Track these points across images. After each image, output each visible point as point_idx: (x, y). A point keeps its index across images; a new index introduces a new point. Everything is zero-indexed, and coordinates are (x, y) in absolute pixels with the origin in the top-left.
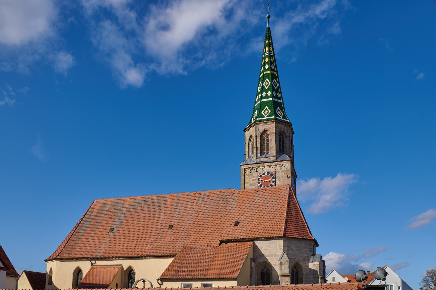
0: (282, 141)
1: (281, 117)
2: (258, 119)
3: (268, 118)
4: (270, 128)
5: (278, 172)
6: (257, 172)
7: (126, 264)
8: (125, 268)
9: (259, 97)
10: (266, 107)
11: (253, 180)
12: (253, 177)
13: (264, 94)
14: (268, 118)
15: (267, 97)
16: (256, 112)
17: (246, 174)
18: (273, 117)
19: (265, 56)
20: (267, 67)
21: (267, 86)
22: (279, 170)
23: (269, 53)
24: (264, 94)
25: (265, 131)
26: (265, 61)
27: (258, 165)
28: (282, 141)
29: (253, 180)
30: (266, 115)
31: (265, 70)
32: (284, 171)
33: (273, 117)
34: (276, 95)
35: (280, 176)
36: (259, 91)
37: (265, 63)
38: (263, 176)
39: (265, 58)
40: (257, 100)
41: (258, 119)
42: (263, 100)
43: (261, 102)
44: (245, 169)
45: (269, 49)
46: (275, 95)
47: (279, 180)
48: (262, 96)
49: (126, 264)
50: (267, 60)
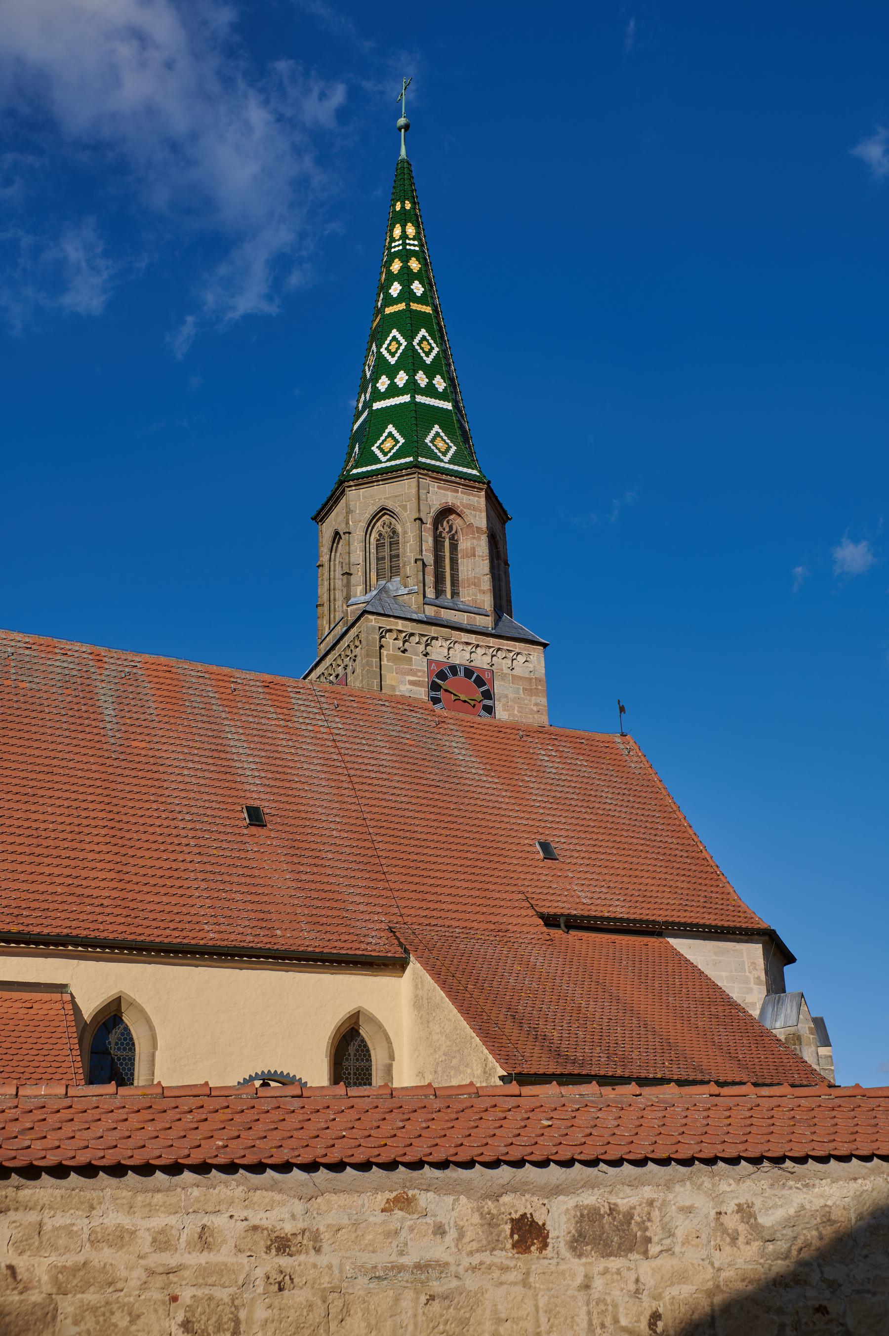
3: (393, 463)
4: (469, 506)
5: (504, 677)
6: (426, 655)
7: (92, 984)
8: (89, 1008)
10: (391, 428)
11: (412, 683)
12: (412, 672)
13: (383, 384)
15: (393, 391)
17: (384, 652)
18: (411, 459)
20: (395, 289)
21: (427, 354)
22: (506, 671)
23: (404, 244)
24: (383, 384)
25: (446, 512)
26: (389, 272)
27: (433, 631)
29: (412, 683)
30: (385, 454)
31: (390, 301)
32: (521, 678)
34: (430, 385)
35: (511, 696)
37: (392, 278)
38: (450, 675)
39: (390, 262)
40: (360, 405)
41: (355, 471)
43: (413, 402)
44: (384, 633)
45: (404, 231)
47: (506, 708)
48: (375, 390)
49: (92, 984)
50: (396, 266)
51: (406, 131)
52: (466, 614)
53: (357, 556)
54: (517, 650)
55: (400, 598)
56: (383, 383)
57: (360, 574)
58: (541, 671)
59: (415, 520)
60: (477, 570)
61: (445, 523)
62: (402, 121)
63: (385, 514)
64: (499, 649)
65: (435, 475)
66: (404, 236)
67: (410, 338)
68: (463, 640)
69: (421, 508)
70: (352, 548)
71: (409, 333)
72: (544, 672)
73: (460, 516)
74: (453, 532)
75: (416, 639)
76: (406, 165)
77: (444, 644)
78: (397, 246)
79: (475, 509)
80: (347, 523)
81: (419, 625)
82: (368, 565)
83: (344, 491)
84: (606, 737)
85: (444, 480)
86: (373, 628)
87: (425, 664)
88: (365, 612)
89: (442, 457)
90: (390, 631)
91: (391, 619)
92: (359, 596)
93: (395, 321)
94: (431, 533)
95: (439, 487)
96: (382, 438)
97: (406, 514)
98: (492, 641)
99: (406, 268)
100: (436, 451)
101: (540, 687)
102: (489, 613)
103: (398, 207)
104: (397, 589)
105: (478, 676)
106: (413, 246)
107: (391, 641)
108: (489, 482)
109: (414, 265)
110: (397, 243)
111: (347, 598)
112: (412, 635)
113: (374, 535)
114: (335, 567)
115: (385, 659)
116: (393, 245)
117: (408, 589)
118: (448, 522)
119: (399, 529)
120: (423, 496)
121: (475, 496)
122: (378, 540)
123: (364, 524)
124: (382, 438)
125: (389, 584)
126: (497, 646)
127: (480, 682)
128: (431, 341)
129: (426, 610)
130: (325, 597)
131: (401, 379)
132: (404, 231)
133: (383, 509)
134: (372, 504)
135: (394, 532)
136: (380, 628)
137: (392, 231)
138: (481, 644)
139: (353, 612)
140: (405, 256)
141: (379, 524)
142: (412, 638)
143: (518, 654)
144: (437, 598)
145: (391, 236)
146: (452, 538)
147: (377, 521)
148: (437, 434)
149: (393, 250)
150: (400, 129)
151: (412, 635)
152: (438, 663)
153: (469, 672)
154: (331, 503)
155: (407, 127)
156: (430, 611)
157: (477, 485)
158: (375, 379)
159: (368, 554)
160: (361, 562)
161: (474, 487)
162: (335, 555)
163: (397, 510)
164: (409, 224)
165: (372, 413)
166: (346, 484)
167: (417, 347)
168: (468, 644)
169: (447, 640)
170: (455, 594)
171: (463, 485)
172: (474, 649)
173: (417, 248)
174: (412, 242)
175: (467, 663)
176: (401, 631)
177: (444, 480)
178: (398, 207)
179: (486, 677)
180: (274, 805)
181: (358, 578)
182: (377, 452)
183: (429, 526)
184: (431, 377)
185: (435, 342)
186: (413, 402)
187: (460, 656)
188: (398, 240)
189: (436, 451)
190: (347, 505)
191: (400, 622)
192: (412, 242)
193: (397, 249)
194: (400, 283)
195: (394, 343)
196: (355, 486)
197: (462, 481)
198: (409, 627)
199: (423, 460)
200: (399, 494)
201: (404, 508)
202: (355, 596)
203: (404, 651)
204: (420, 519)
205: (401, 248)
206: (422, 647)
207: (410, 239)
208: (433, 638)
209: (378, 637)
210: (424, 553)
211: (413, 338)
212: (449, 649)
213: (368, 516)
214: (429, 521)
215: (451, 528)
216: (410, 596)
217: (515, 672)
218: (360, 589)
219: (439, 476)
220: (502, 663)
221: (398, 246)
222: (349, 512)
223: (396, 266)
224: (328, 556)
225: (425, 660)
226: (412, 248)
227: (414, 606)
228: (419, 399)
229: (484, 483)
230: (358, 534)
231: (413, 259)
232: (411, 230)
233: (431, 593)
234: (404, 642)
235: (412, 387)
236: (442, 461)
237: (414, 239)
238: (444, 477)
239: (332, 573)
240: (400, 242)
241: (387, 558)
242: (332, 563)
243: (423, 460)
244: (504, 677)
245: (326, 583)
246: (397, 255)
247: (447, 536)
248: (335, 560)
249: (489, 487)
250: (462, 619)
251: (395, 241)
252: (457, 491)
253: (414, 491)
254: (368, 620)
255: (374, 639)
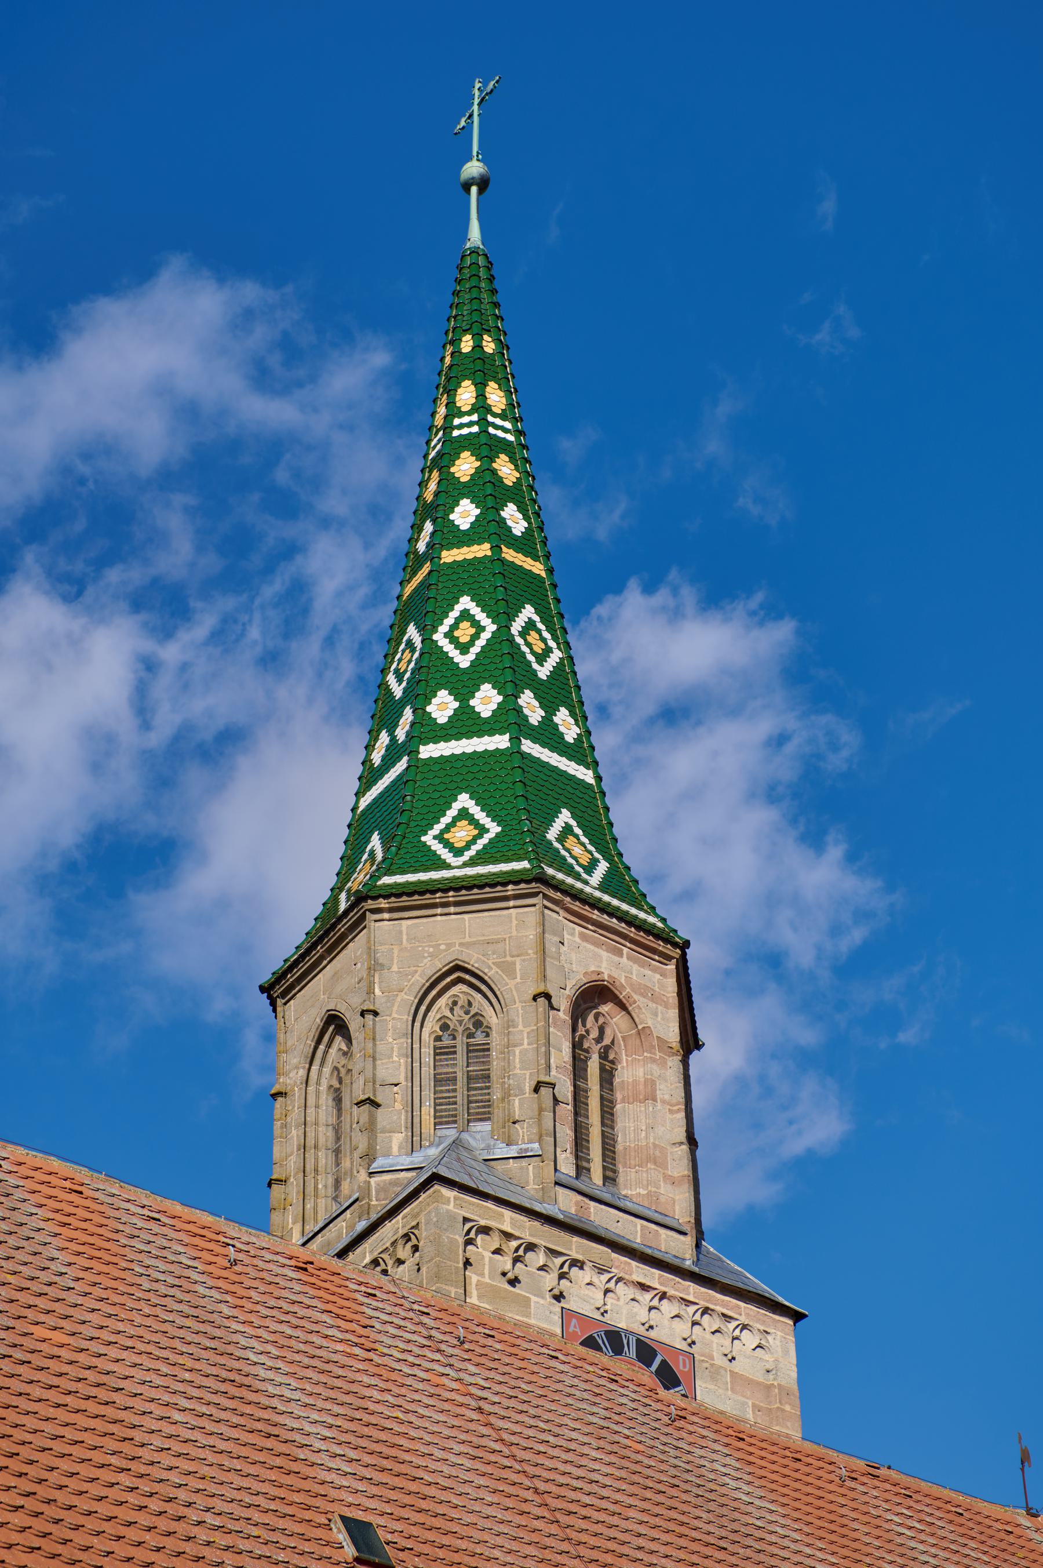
0: (593, 1065)
1: (596, 878)
2: (387, 880)
4: (645, 991)
5: (715, 1373)
6: (559, 1297)
9: (401, 734)
14: (598, 894)
15: (466, 723)
16: (375, 842)
18: (525, 864)
19: (447, 440)
20: (465, 514)
21: (465, 615)
23: (483, 422)
24: (442, 706)
25: (596, 994)
27: (575, 1246)
28: (593, 1065)
30: (458, 852)
32: (750, 1382)
33: (525, 864)
34: (548, 722)
36: (398, 691)
37: (452, 491)
40: (377, 758)
41: (387, 880)
42: (428, 751)
43: (515, 751)
45: (481, 396)
46: (535, 715)
50: (465, 466)
51: (481, 192)
52: (640, 1222)
53: (393, 1065)
54: (743, 1319)
55: (499, 1166)
56: (443, 706)
57: (398, 1106)
58: (789, 1372)
59: (535, 999)
60: (660, 1130)
61: (590, 1018)
62: (473, 168)
63: (459, 980)
64: (706, 1311)
65: (576, 906)
66: (481, 406)
67: (504, 616)
68: (636, 1278)
69: (548, 973)
70: (381, 1047)
71: (502, 607)
72: (794, 1375)
73: (623, 1006)
74: (607, 1041)
75: (541, 1258)
76: (481, 261)
77: (595, 1280)
78: (465, 426)
79: (654, 998)
80: (370, 991)
81: (547, 1228)
82: (416, 1089)
83: (363, 918)
84: (996, 1511)
85: (595, 923)
86: (452, 1217)
87: (557, 1318)
88: (436, 1178)
89: (584, 876)
90: (485, 1230)
91: (490, 1205)
92: (398, 1155)
93: (465, 579)
94: (568, 1031)
95: (583, 937)
96: (446, 820)
97: (512, 984)
98: (693, 1290)
99: (486, 476)
100: (570, 860)
101: (788, 1408)
102: (686, 1228)
103: (467, 344)
104: (488, 1148)
105: (664, 1362)
106: (503, 430)
107: (487, 1255)
108: (687, 944)
109: (506, 470)
110: (466, 419)
111: (369, 1157)
112: (531, 1247)
113: (432, 1025)
114: (318, 1097)
115: (475, 1293)
116: (457, 421)
117: (521, 1147)
118: (597, 1017)
119: (491, 1018)
120: (551, 949)
121: (655, 970)
122: (438, 1039)
123: (410, 998)
124: (446, 820)
125: (465, 1136)
126: (703, 1304)
127: (668, 1377)
128: (546, 635)
129: (560, 1199)
130: (293, 1163)
131: (486, 700)
132: (481, 396)
133: (458, 968)
134: (431, 955)
135: (478, 1023)
136: (466, 1220)
137: (451, 392)
138: (671, 1292)
139: (382, 1189)
140: (486, 447)
141: (442, 1001)
142: (530, 1255)
143: (745, 1327)
144: (577, 1178)
145: (451, 404)
146: (604, 1056)
147: (440, 995)
148: (483, 830)
149: (456, 433)
150: (466, 187)
151: (531, 1247)
152: (582, 1318)
153: (646, 1352)
154: (320, 949)
155: (483, 184)
156: (566, 1204)
157: (660, 945)
158: (419, 694)
159: (416, 1065)
160: (402, 1078)
161: (654, 951)
162: (320, 1072)
163: (491, 973)
164: (492, 385)
165: (415, 765)
166: (370, 904)
167: (519, 640)
168: (644, 1287)
169: (601, 1271)
170: (610, 1178)
171: (633, 941)
172: (655, 1302)
173: (510, 438)
174: (498, 421)
175: (641, 1330)
176: (508, 1236)
177: (595, 923)
178: (467, 344)
179: (680, 1368)
180: (398, 1526)
181: (393, 1112)
182: (437, 847)
183: (563, 1015)
184: (550, 710)
185: (555, 638)
186: (515, 751)
187: (627, 1313)
188: (469, 413)
189: (570, 860)
190: (370, 951)
191: (508, 1214)
192: (498, 421)
193: (465, 431)
194: (477, 501)
195: (465, 624)
196: (391, 910)
197: (632, 932)
198: (527, 1229)
199: (550, 871)
200: (504, 938)
201: (509, 969)
202: (387, 1154)
203: (514, 1282)
204: (548, 996)
205: (475, 429)
206: (550, 1280)
207: (495, 415)
208: (576, 1263)
209: (461, 1240)
210: (553, 1072)
211: (511, 617)
212: (607, 1291)
213: (419, 980)
214: (563, 1002)
215: (602, 1030)
216: (524, 1162)
217: (736, 1366)
218: (398, 1140)
219: (586, 911)
220: (711, 1345)
221: (470, 424)
222: (374, 967)
223: (465, 466)
224: (302, 1073)
225: (557, 1307)
226: (500, 434)
227: (532, 1187)
228: (528, 746)
229: (675, 945)
230: (396, 1015)
231: (503, 457)
232: (496, 397)
233: (567, 1168)
234: (516, 1260)
235: (508, 718)
236: (586, 883)
237: (503, 416)
238: (596, 915)
239: (311, 1111)
240: (475, 417)
241: (464, 1077)
242: (311, 1089)
243: (550, 871)
244: (715, 1373)
245: (295, 1133)
246: (467, 443)
247: (596, 1048)
248: (318, 1083)
249: (684, 955)
250: (634, 1232)
251: (461, 414)
252: (620, 954)
253: (531, 934)
254: (439, 1199)
255: (453, 1241)
